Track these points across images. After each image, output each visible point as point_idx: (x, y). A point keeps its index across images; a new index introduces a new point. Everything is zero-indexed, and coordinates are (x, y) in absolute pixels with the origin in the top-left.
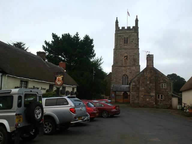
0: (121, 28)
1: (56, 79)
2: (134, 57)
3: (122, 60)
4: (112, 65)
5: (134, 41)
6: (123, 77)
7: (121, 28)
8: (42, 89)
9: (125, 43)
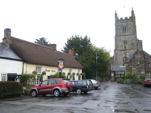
0: (120, 19)
1: (59, 64)
2: (132, 42)
3: (122, 45)
4: (114, 50)
5: (131, 29)
6: (123, 59)
7: (120, 19)
8: (52, 71)
9: (123, 30)
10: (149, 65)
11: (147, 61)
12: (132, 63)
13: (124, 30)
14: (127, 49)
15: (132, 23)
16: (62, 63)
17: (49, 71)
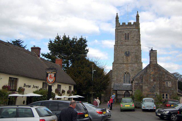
5: (135, 38)
7: (121, 24)
8: (34, 87)
9: (126, 39)
10: (164, 83)
11: (161, 78)
12: (144, 80)
13: (127, 38)
14: (129, 63)
15: (137, 30)
16: (52, 74)
17: (29, 86)
